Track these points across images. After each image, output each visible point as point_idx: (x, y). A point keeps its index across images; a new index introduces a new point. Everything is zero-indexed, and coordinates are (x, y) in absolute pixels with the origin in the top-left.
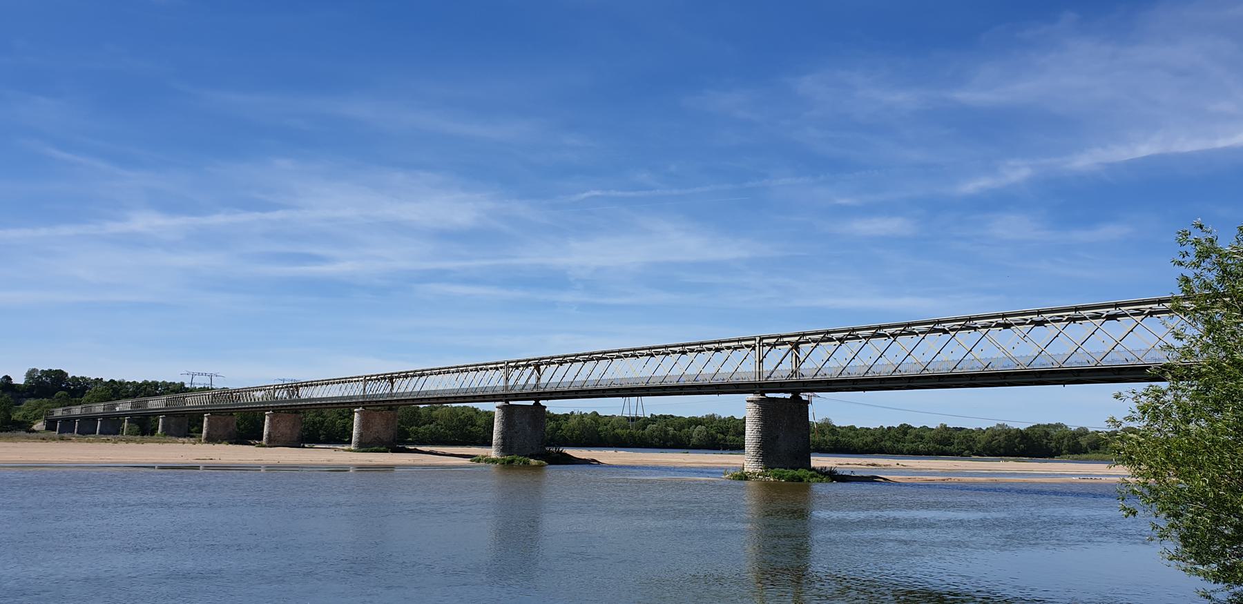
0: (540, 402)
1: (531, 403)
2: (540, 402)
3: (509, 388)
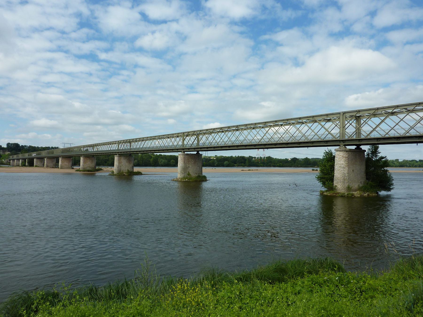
0: (200, 152)
1: (195, 153)
2: (200, 152)
3: (185, 146)
